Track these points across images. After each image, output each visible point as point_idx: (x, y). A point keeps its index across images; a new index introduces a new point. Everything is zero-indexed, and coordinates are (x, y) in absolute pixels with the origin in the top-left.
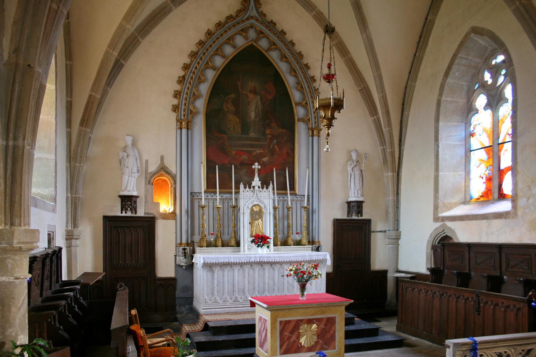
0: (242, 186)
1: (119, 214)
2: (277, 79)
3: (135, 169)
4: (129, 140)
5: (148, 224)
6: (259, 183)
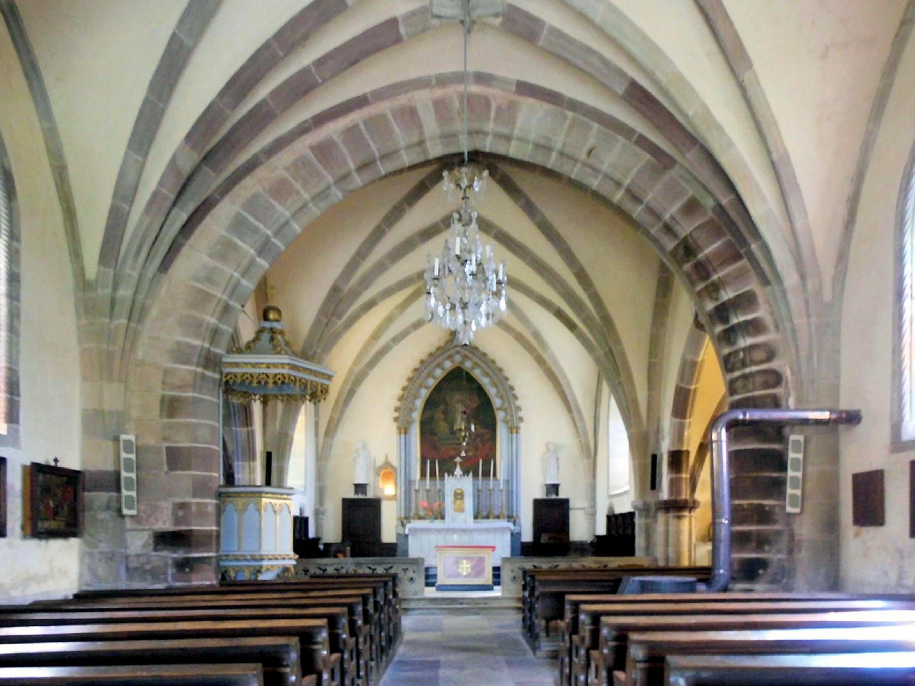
0: (446, 475)
2: (480, 391)
4: (360, 444)
5: (374, 506)
6: (461, 473)
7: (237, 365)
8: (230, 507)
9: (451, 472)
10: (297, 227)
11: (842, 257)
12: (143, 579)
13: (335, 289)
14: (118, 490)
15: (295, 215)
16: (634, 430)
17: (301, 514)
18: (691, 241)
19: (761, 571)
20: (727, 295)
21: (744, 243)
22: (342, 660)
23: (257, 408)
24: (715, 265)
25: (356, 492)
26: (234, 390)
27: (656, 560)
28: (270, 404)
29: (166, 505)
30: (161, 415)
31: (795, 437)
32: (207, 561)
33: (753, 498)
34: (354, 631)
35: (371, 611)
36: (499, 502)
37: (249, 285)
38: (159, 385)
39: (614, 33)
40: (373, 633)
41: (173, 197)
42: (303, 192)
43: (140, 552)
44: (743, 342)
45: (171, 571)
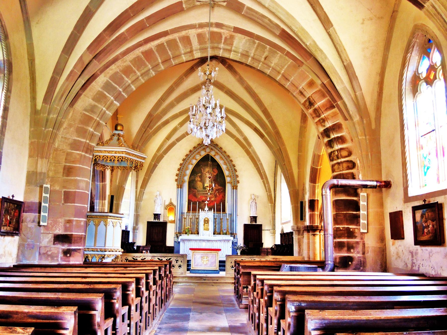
0: (200, 210)
1: (153, 221)
2: (219, 167)
3: (160, 204)
4: (158, 193)
5: (164, 225)
6: (208, 209)
7: (101, 151)
8: (92, 223)
9: (203, 209)
10: (133, 88)
11: (378, 109)
12: (47, 259)
13: (150, 115)
14: (40, 212)
15: (132, 82)
16: (292, 189)
17: (126, 229)
18: (311, 99)
19: (350, 263)
20: (328, 124)
21: (335, 101)
22: (141, 302)
23: (108, 173)
24: (323, 110)
25: (155, 218)
26: (99, 164)
27: (304, 258)
28: (115, 171)
29: (62, 221)
30: (63, 175)
31: (363, 194)
32: (79, 251)
33: (345, 225)
34: (148, 288)
35: (157, 279)
36: (226, 225)
37: (110, 114)
38: (64, 160)
39: (274, 11)
40: (157, 291)
41: (79, 73)
42: (137, 72)
43: (46, 245)
44: (337, 147)
45: (61, 255)
